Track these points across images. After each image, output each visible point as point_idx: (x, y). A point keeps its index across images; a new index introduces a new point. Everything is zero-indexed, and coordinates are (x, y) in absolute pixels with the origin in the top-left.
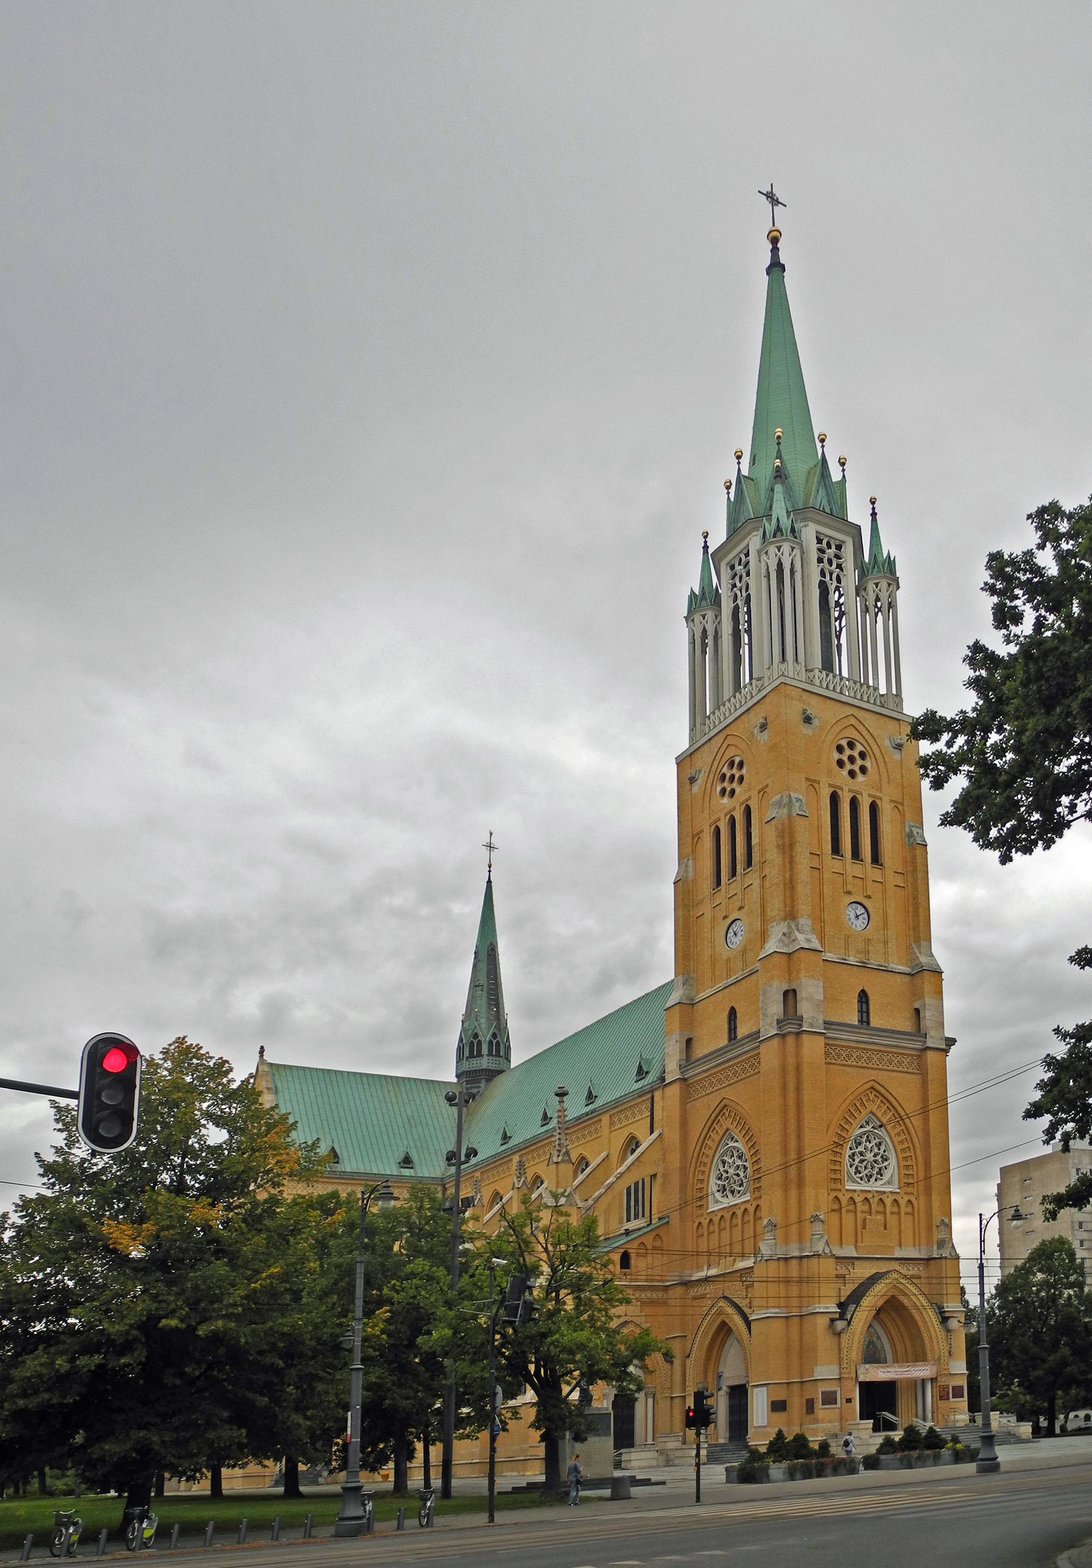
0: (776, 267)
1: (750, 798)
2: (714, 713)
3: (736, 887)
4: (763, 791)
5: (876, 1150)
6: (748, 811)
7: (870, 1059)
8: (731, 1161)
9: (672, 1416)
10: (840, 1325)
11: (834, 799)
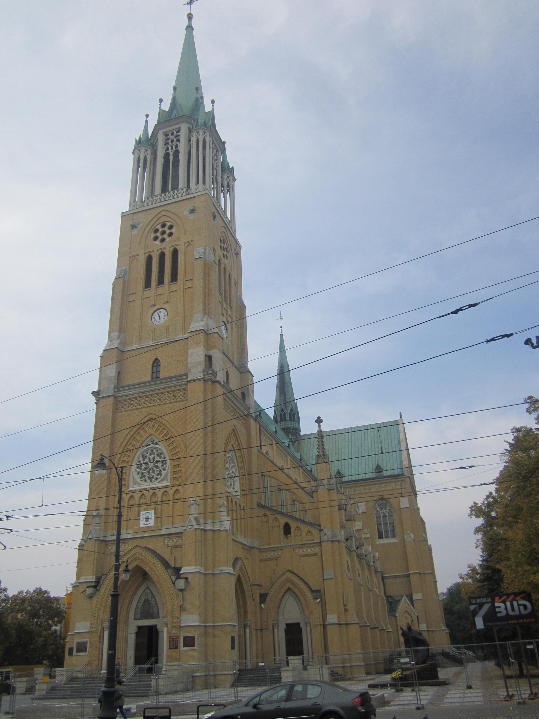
0: (190, 28)
1: (178, 245)
2: (148, 199)
4: (189, 243)
5: (146, 460)
6: (175, 253)
9: (262, 643)
10: (90, 591)
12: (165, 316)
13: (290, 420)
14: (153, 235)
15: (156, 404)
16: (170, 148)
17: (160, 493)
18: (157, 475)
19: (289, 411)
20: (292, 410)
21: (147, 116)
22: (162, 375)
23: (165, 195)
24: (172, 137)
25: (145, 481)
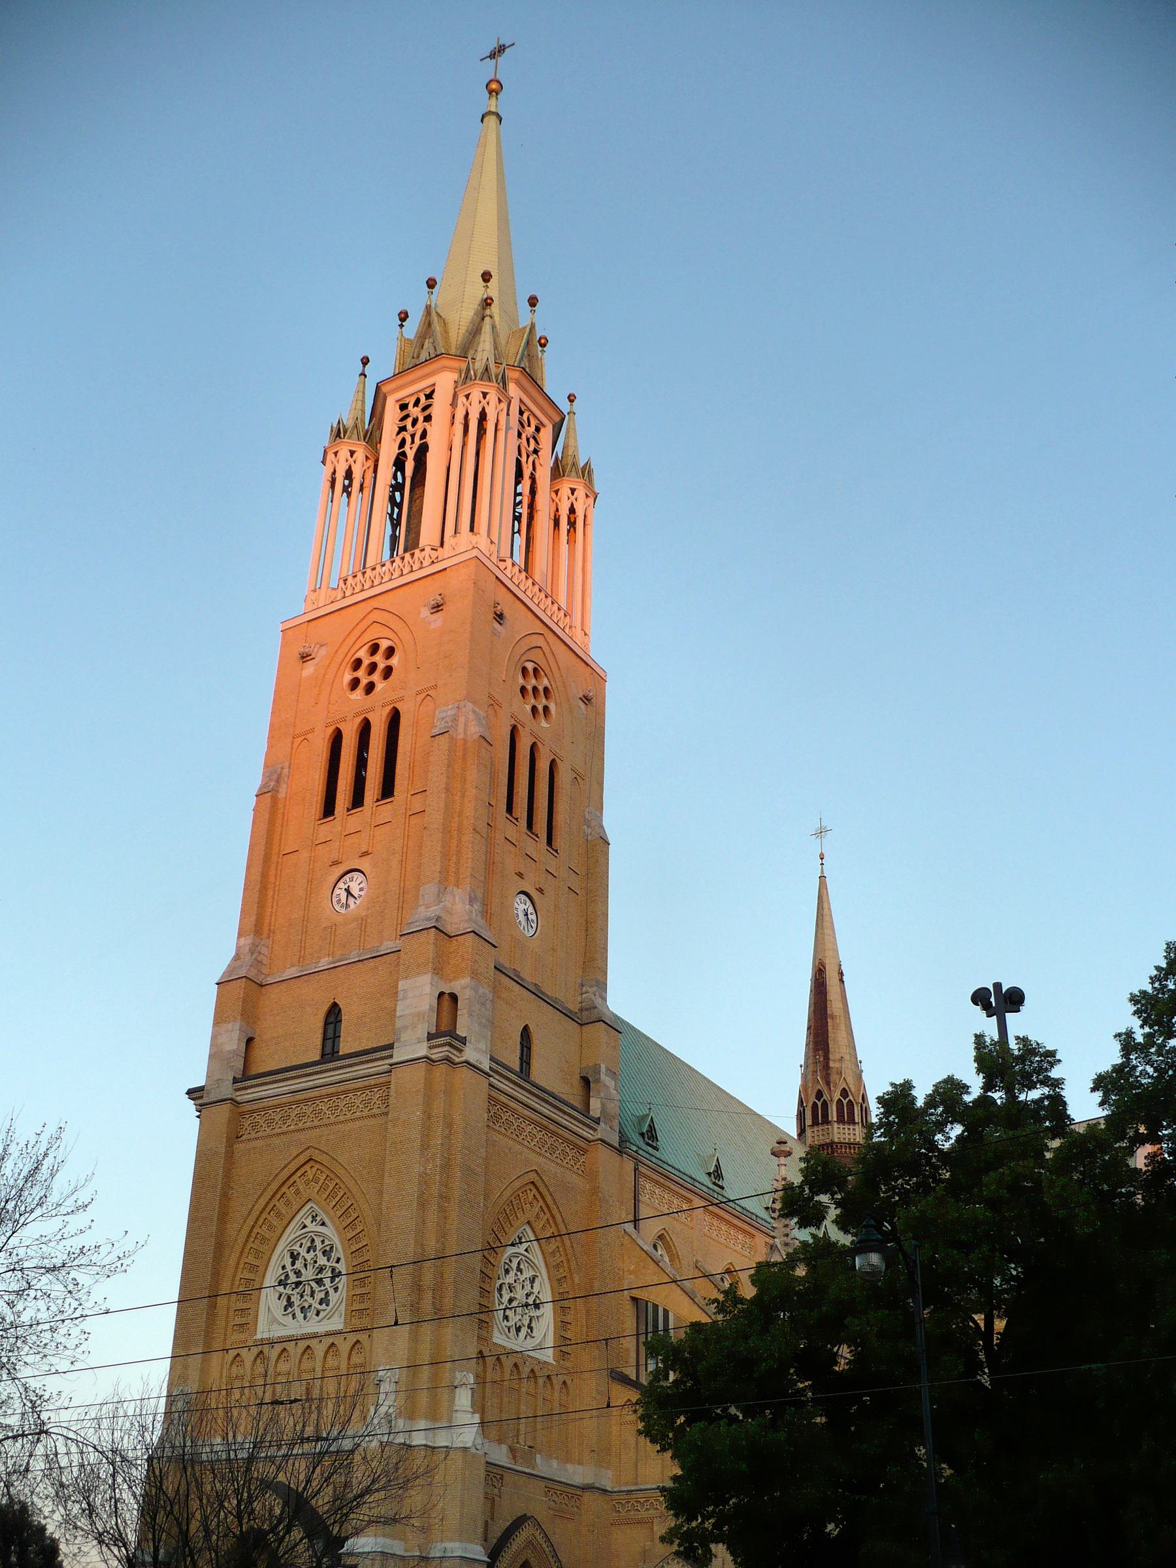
1: (401, 699)
3: (387, 810)
6: (395, 719)
7: (318, 1113)
8: (309, 1257)
11: (514, 731)
12: (361, 890)
13: (841, 1120)
14: (348, 677)
15: (325, 1121)
16: (409, 440)
17: (319, 1349)
18: (320, 1304)
19: (837, 1096)
20: (844, 1093)
21: (365, 361)
22: (344, 1048)
23: (412, 555)
24: (415, 412)
25: (294, 1316)
